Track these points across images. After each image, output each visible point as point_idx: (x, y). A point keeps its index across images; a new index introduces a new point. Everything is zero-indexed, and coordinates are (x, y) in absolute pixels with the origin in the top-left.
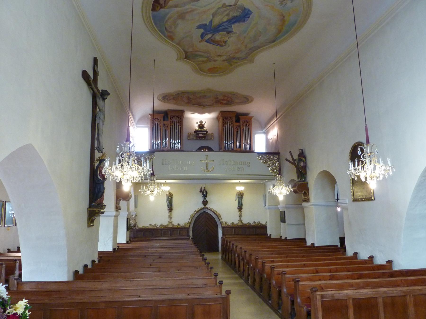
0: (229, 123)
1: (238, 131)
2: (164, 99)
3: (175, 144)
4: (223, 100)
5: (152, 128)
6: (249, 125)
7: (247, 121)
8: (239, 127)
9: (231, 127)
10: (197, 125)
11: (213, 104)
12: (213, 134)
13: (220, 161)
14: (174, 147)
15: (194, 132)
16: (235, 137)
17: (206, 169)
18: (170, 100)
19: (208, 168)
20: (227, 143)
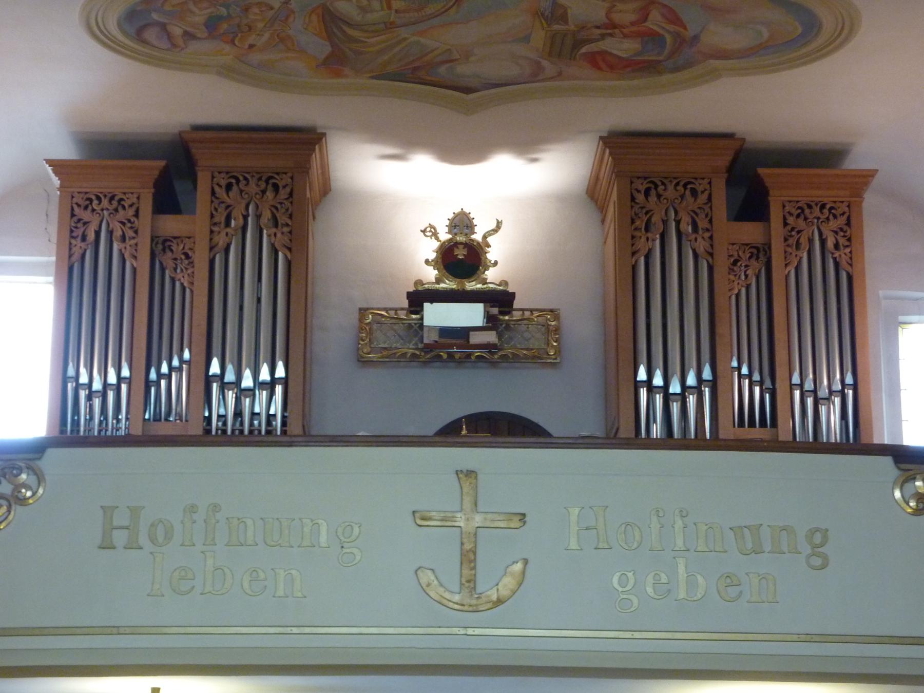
0: (678, 223)
1: (748, 288)
2: (139, 36)
3: (242, 393)
4: (611, 27)
5: (71, 269)
6: (842, 241)
7: (829, 210)
8: (762, 258)
9: (696, 256)
10: (429, 249)
11: (536, 75)
12: (557, 317)
13: (574, 518)
14: (238, 414)
15: (405, 303)
16: (727, 330)
17: (457, 589)
18: (189, 36)
19: (472, 581)
20: (658, 381)
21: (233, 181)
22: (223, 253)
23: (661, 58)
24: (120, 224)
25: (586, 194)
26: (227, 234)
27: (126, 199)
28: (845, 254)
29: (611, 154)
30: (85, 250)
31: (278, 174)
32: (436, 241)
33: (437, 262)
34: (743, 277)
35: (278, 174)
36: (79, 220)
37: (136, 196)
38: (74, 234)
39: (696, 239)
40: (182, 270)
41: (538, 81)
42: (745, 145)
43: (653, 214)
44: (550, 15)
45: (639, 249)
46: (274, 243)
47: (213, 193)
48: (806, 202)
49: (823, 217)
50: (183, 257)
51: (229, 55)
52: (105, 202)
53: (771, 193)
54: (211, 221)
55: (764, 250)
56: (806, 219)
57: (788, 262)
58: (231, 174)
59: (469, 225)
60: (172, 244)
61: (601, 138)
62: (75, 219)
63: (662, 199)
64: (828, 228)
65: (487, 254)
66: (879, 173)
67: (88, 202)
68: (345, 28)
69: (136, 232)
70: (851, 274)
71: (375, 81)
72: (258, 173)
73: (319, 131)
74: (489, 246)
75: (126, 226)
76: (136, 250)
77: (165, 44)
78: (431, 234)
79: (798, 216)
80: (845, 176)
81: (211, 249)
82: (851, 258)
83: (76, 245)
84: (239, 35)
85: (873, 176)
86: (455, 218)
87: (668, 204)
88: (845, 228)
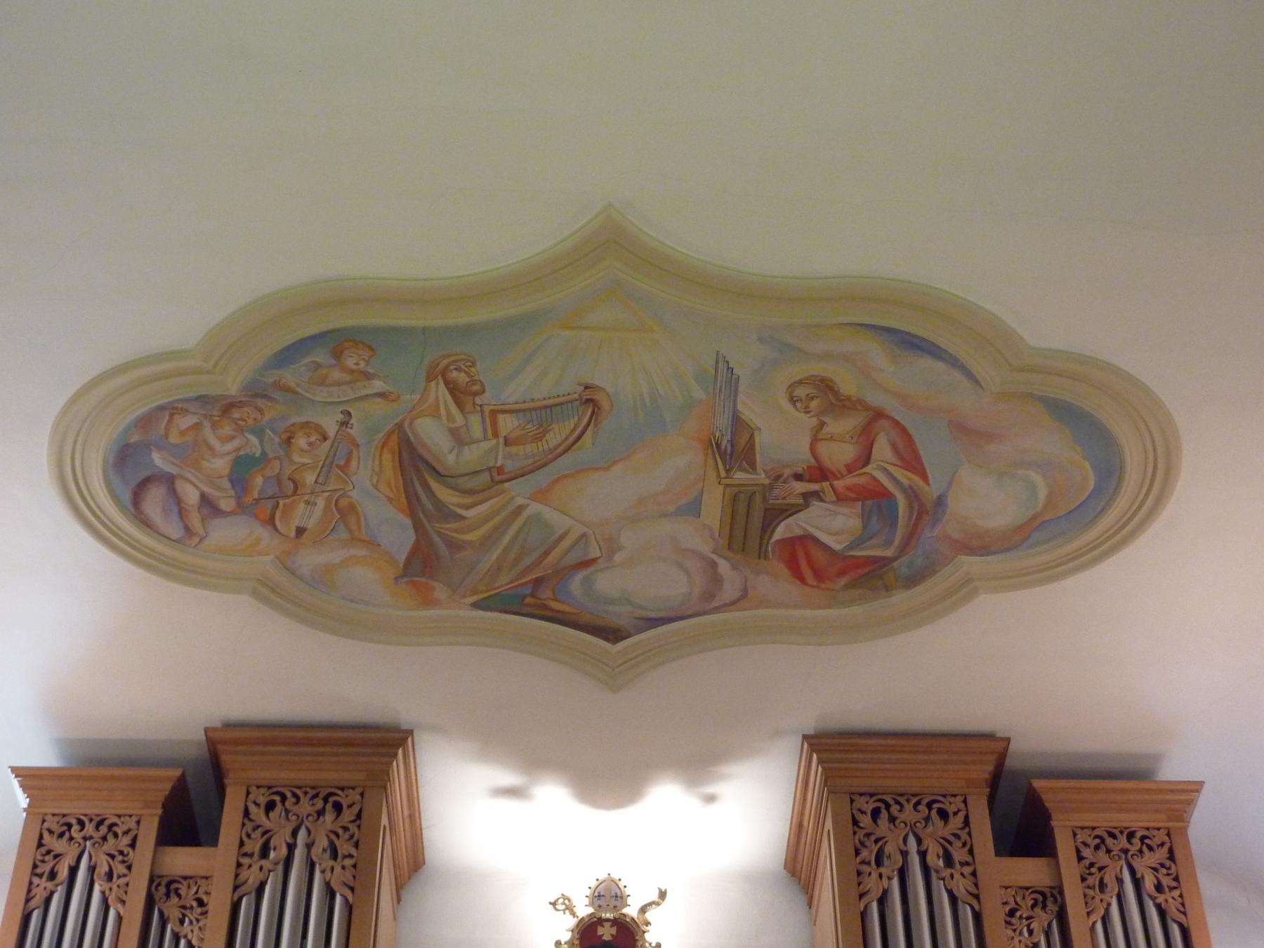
0: (923, 855)
6: (1166, 881)
9: (953, 900)
21: (277, 798)
22: (253, 894)
23: (889, 553)
24: (107, 857)
25: (785, 868)
26: (261, 868)
27: (120, 824)
28: (1173, 898)
29: (820, 762)
30: (52, 893)
31: (342, 789)
32: (572, 917)
33: (573, 944)
34: (1026, 934)
35: (342, 789)
36: (49, 852)
37: (134, 819)
38: (38, 871)
39: (952, 876)
40: (191, 922)
41: (717, 610)
42: (1010, 763)
43: (887, 842)
44: (729, 449)
45: (869, 890)
46: (330, 880)
47: (247, 813)
48: (1107, 829)
49: (1133, 850)
50: (195, 904)
51: (267, 555)
52: (90, 829)
53: (1054, 816)
54: (239, 850)
55: (1053, 895)
56: (1108, 851)
57: (1090, 909)
58: (275, 790)
59: (619, 894)
60: (180, 886)
61: (806, 737)
62: (43, 850)
63: (897, 822)
64: (1142, 864)
65: (646, 934)
66: (1205, 786)
67: (65, 828)
68: (434, 484)
69: (129, 868)
70: (1186, 925)
71: (481, 613)
72: (313, 788)
73: (404, 727)
74: (648, 924)
75: (115, 859)
76: (126, 892)
77: (175, 531)
78: (564, 907)
79: (1097, 847)
80: (1160, 791)
81: (236, 888)
82: (1183, 904)
83: (38, 885)
84: (281, 502)
85: (1198, 791)
86: (598, 886)
87: (907, 830)
88: (1168, 863)
